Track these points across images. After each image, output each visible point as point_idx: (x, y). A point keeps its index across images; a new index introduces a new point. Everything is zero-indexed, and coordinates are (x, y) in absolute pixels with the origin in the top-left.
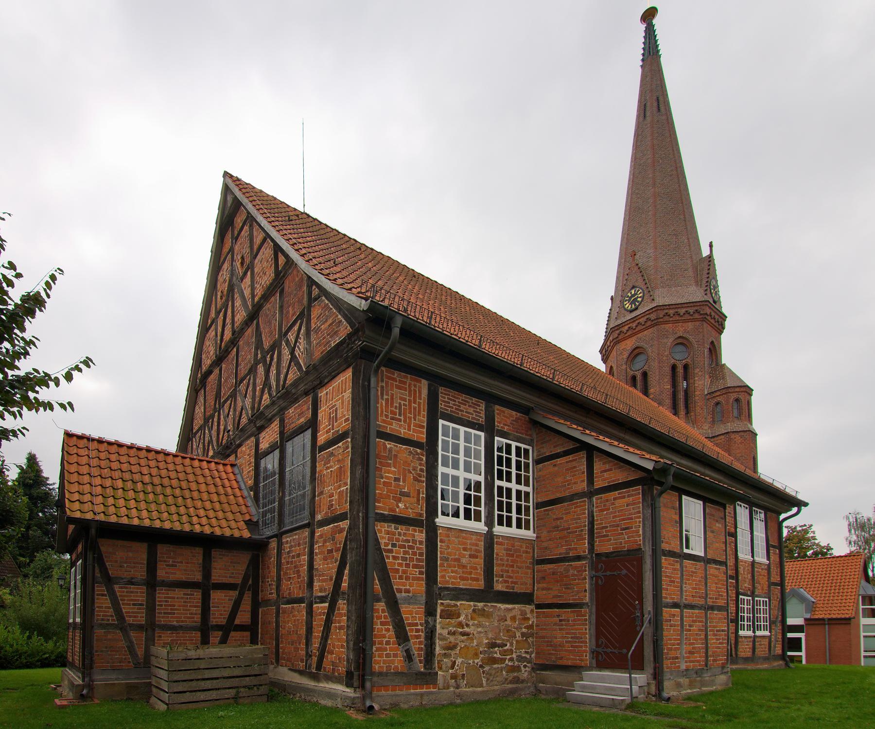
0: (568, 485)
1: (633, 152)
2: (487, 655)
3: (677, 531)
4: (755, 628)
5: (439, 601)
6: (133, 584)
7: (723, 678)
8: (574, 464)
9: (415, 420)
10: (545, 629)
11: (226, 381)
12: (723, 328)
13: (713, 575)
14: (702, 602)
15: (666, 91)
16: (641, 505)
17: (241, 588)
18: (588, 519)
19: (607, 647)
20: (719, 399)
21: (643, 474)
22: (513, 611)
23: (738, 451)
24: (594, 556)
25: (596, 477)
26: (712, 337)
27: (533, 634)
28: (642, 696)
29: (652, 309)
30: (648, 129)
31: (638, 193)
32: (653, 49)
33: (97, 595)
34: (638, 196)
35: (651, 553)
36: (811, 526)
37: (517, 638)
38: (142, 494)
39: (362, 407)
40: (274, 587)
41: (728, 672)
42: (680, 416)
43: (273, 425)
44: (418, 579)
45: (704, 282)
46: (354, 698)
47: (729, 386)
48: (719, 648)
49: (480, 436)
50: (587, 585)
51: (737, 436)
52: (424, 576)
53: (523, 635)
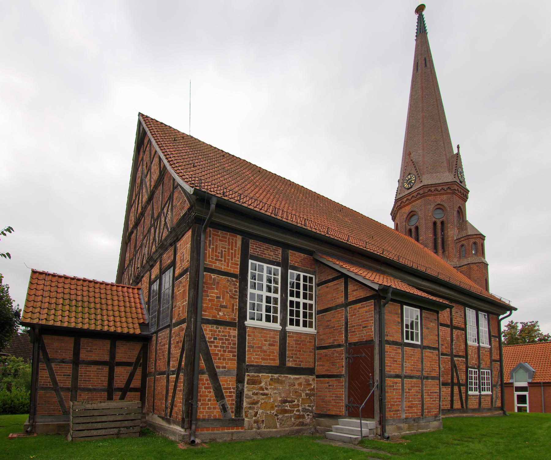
0: (334, 299)
2: (280, 408)
3: (399, 328)
5: (246, 374)
6: (64, 362)
7: (436, 423)
8: (338, 286)
9: (232, 260)
10: (321, 391)
11: (139, 238)
12: (467, 198)
13: (428, 357)
14: (419, 374)
17: (135, 365)
18: (345, 321)
20: (463, 242)
21: (375, 293)
25: (350, 294)
27: (314, 394)
30: (419, 77)
33: (41, 369)
34: (413, 118)
35: (378, 343)
36: (537, 322)
38: (87, 309)
39: (195, 253)
40: (154, 364)
41: (439, 420)
43: (157, 264)
44: (232, 360)
45: (454, 170)
46: (184, 435)
47: (469, 234)
49: (278, 270)
50: (344, 363)
51: (475, 266)
52: (236, 358)
53: (307, 395)
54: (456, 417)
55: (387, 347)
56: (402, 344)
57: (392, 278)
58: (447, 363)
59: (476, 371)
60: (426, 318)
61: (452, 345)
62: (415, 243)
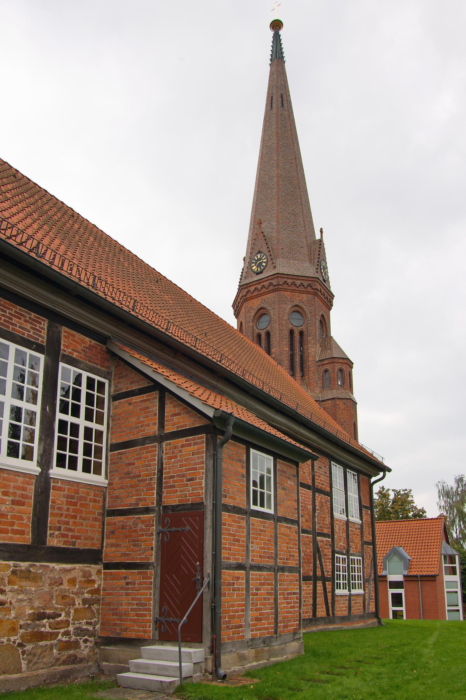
0: (141, 426)
1: (262, 134)
2: (30, 630)
3: (244, 485)
4: (350, 586)
7: (294, 645)
8: (148, 404)
14: (271, 563)
15: (289, 92)
16: (204, 454)
18: (158, 467)
19: (169, 615)
22: (73, 572)
23: (342, 417)
24: (161, 509)
25: (167, 421)
26: (322, 310)
27: (99, 600)
28: (198, 674)
29: (274, 275)
30: (274, 118)
31: (265, 171)
32: (278, 54)
35: (211, 508)
36: (411, 490)
37: (77, 606)
41: (300, 638)
42: (297, 378)
45: (316, 261)
47: (334, 356)
48: (290, 612)
49: (39, 359)
50: (154, 542)
53: (85, 601)
54: (321, 631)
55: (225, 516)
56: (247, 512)
57: (234, 403)
58: (308, 544)
59: (345, 558)
60: (282, 471)
61: (314, 517)
62: (266, 356)
